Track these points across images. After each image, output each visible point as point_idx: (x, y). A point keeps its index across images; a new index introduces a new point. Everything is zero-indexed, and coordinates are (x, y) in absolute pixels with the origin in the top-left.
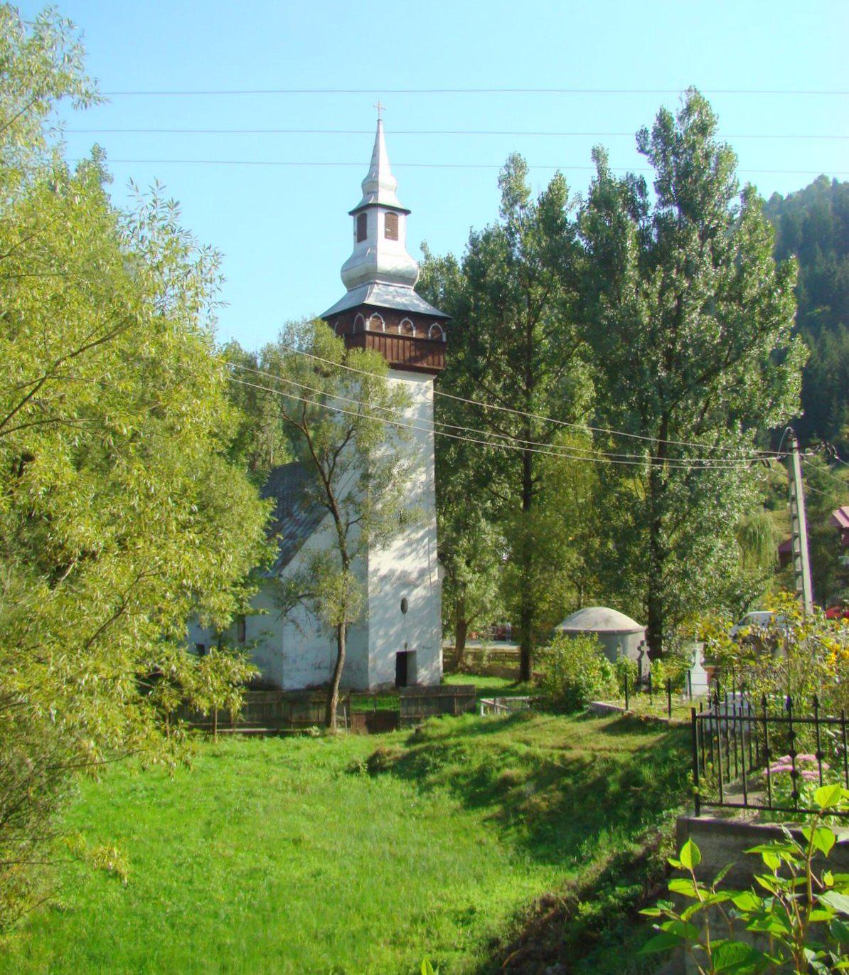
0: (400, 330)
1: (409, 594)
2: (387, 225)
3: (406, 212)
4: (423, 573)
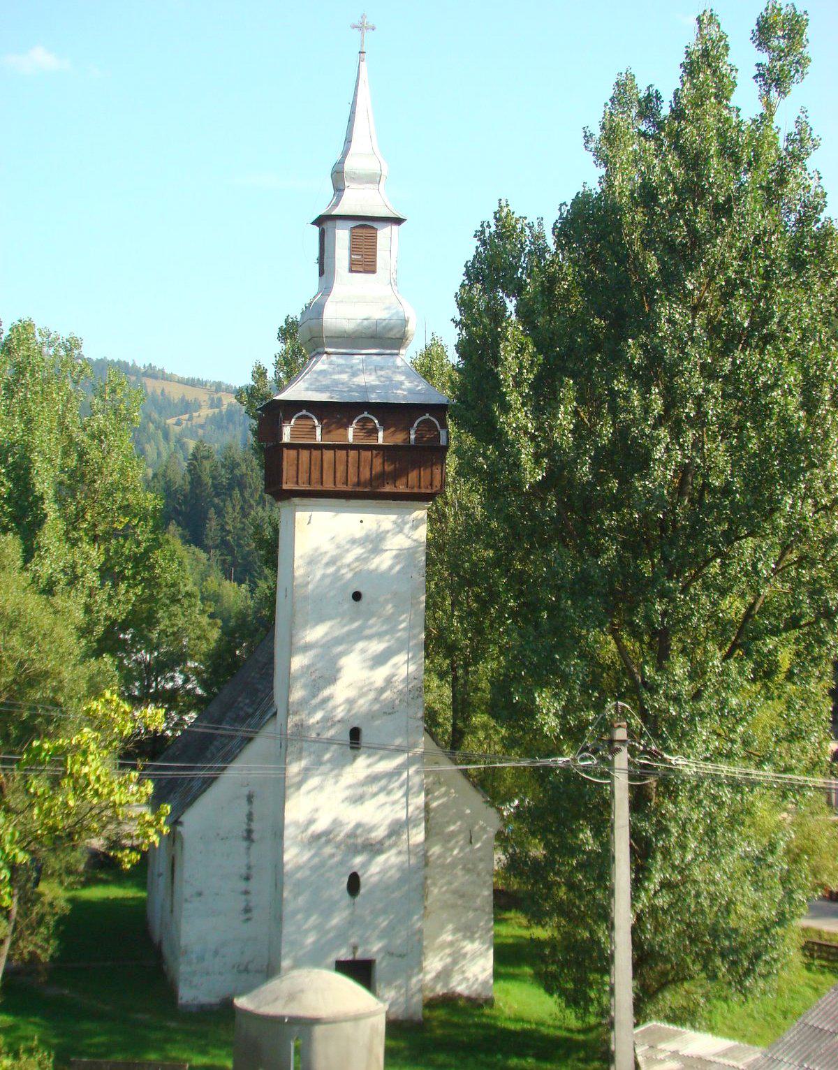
0: (351, 435)
1: (365, 865)
2: (354, 248)
3: (398, 221)
4: (397, 829)
